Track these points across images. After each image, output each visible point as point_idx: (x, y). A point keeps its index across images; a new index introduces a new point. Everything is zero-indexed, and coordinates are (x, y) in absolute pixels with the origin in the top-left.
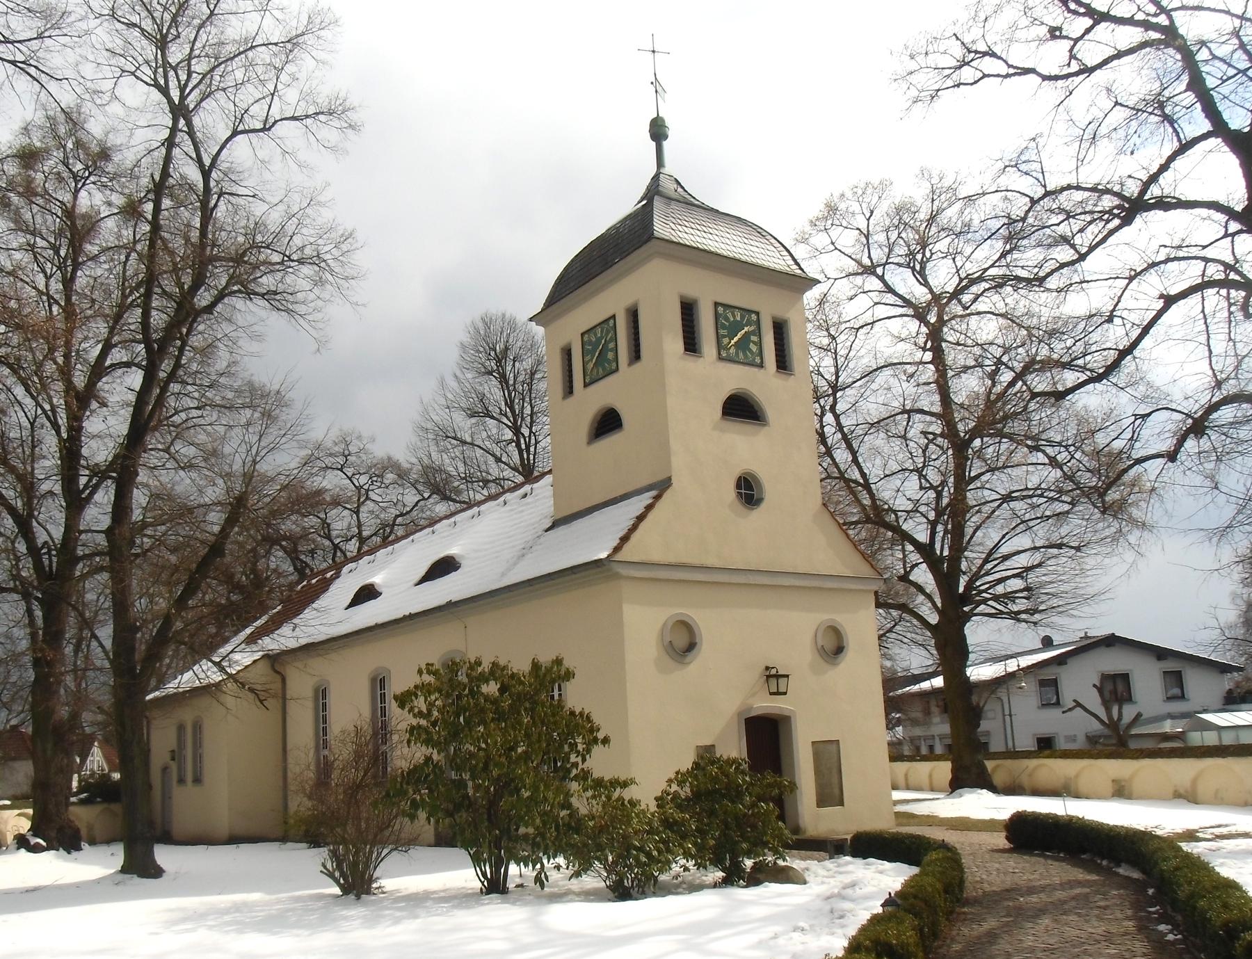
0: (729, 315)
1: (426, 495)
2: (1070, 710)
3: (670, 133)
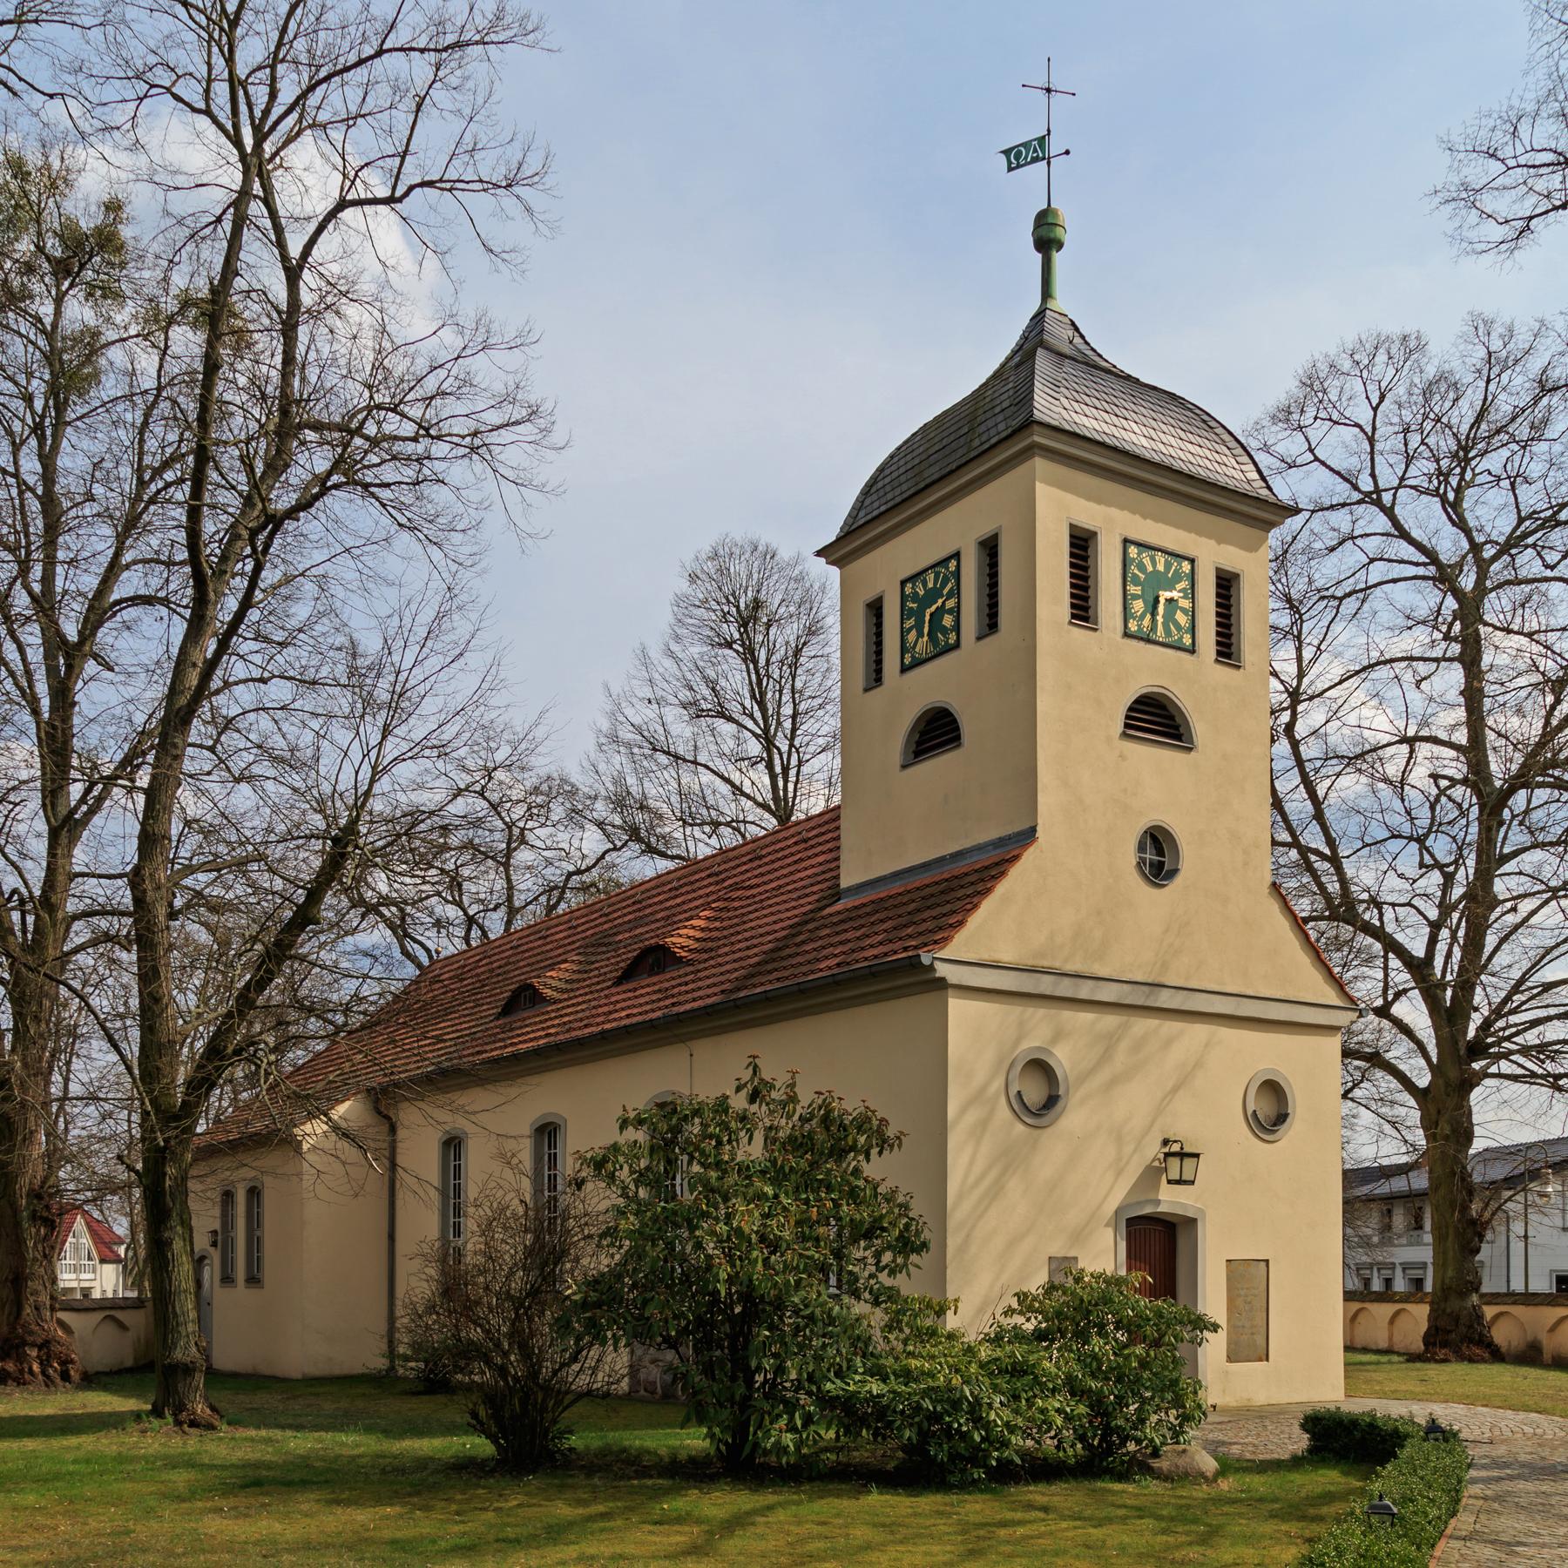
0: (1147, 561)
3: (1067, 239)
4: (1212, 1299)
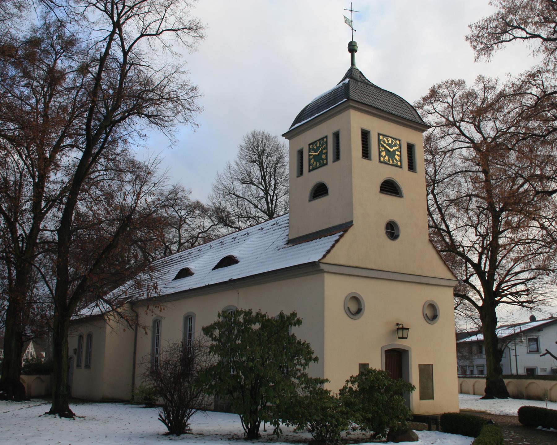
1: (216, 223)
2: (544, 355)
4: (415, 379)
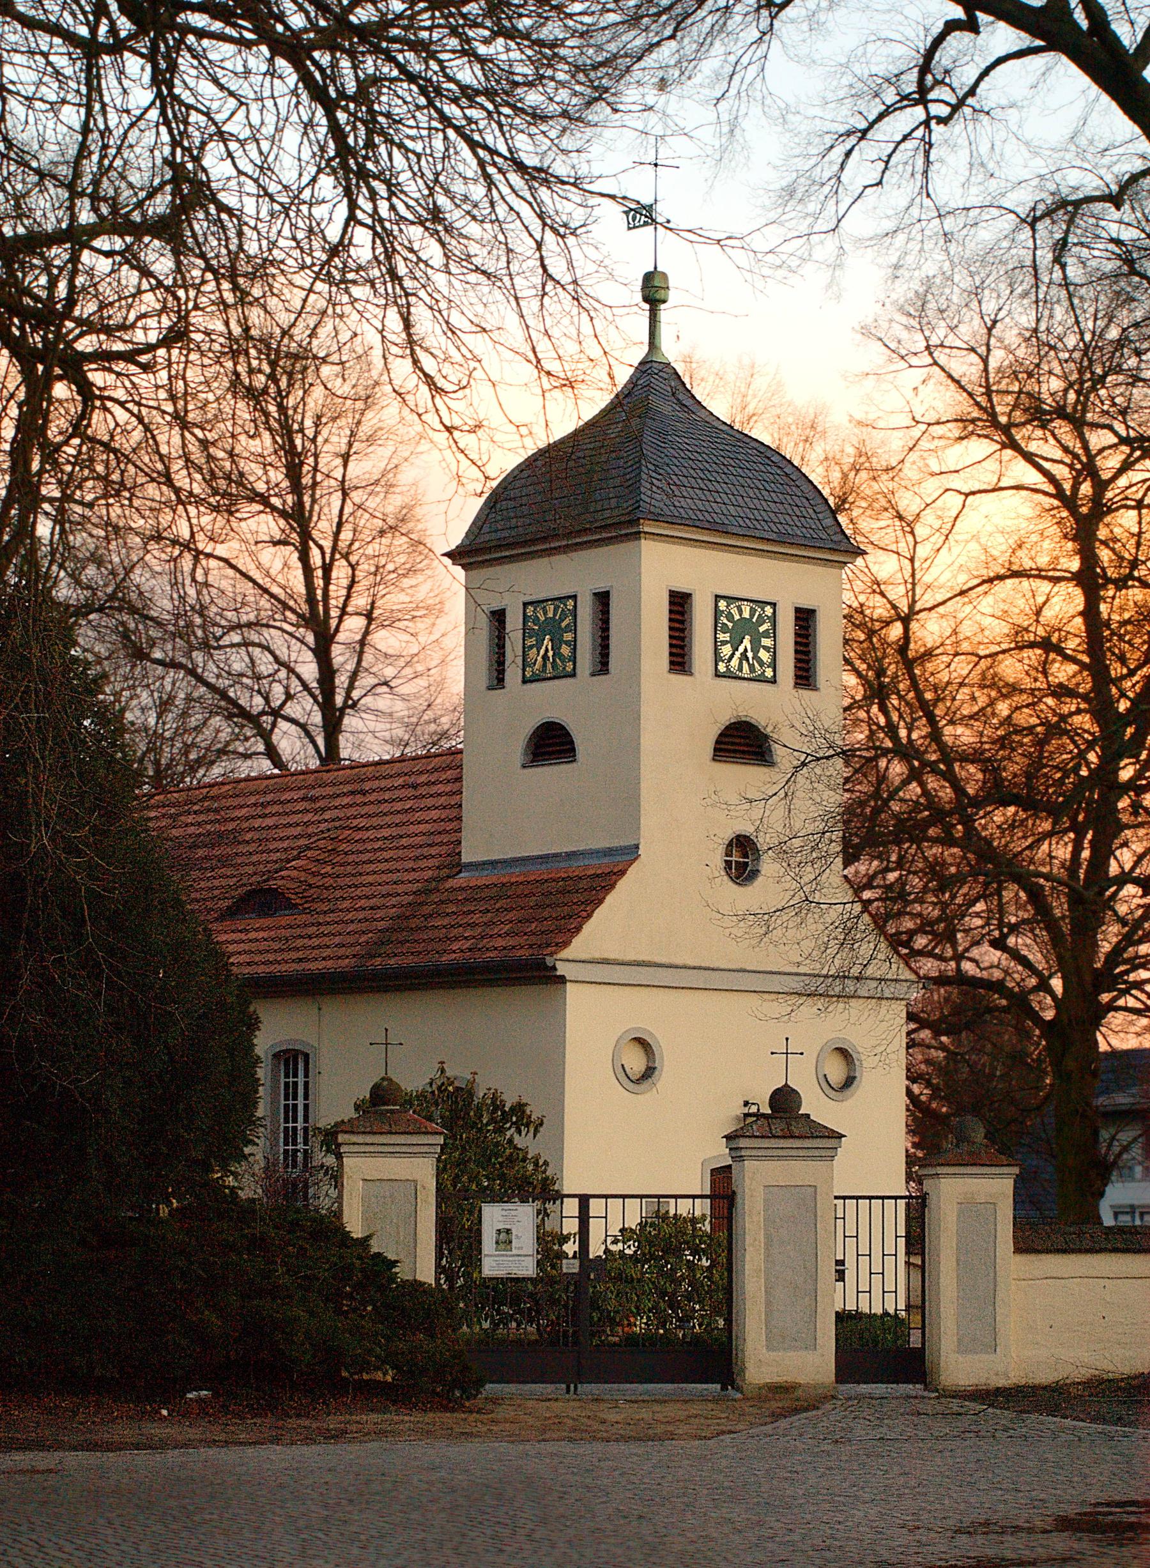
0: (735, 611)
